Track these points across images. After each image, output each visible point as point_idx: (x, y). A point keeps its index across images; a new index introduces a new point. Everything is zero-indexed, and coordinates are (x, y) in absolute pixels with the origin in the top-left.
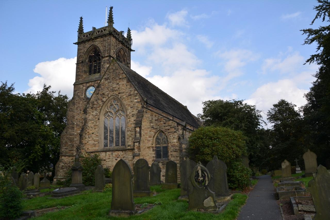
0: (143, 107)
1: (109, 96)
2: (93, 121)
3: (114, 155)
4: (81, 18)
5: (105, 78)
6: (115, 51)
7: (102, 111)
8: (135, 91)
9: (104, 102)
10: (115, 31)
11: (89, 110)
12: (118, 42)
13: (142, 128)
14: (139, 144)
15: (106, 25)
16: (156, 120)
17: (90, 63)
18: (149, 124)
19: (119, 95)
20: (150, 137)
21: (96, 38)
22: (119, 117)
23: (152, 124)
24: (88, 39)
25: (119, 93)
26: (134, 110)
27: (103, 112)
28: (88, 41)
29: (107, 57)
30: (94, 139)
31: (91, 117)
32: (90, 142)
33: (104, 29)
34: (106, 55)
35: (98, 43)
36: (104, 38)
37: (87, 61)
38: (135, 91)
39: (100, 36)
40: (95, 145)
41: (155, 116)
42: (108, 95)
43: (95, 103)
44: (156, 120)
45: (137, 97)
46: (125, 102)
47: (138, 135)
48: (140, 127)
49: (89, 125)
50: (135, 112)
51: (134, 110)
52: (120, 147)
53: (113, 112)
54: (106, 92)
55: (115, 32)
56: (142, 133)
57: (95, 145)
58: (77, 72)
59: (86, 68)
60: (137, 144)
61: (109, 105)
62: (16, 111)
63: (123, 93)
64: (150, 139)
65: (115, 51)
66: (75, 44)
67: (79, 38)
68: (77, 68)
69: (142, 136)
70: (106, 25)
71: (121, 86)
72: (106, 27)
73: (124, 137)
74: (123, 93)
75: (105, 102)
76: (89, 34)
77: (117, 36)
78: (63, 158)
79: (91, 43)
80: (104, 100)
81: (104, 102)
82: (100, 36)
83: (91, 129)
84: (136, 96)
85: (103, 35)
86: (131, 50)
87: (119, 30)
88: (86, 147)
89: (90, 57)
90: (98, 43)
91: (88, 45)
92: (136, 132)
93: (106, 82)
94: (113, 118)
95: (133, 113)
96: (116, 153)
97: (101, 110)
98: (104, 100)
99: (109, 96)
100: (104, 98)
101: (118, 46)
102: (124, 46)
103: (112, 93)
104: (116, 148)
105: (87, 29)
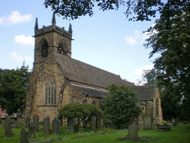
0: (65, 82)
1: (48, 74)
2: (39, 89)
3: (50, 109)
4: (37, 19)
5: (46, 63)
6: (57, 42)
7: (44, 83)
8: (61, 72)
9: (45, 78)
10: (57, 28)
11: (38, 82)
12: (60, 36)
13: (64, 95)
14: (61, 104)
15: (51, 24)
16: (72, 90)
17: (43, 49)
18: (68, 92)
19: (53, 74)
20: (68, 100)
21: (45, 33)
22: (101, 83)
23: (69, 93)
24: (40, 34)
25: (53, 73)
26: (61, 84)
27: (45, 83)
28: (41, 35)
29: (51, 46)
30: (40, 99)
31: (38, 86)
32: (38, 100)
33: (50, 27)
34: (51, 45)
35: (46, 37)
36: (50, 33)
37: (40, 48)
38: (61, 72)
39: (47, 32)
40: (40, 102)
41: (72, 88)
42: (47, 73)
43: (41, 77)
44: (72, 90)
45: (62, 76)
46: (57, 79)
47: (61, 99)
48: (62, 94)
49: (38, 91)
50: (61, 85)
51: (61, 84)
52: (54, 104)
53: (50, 84)
54: (46, 71)
55: (57, 29)
56: (64, 97)
57: (40, 102)
58: (35, 56)
59: (40, 54)
60: (60, 104)
61: (48, 79)
62: (173, 30)
63: (55, 73)
64: (68, 101)
65: (57, 42)
66: (33, 37)
67: (35, 32)
68: (35, 53)
69: (64, 99)
70: (51, 24)
71: (54, 68)
72: (51, 26)
73: (56, 99)
74: (55, 73)
75: (46, 77)
76: (41, 30)
77: (59, 31)
78: (27, 108)
79: (42, 36)
80: (45, 76)
81: (45, 78)
82: (47, 32)
83: (38, 93)
84: (62, 75)
85: (49, 32)
86: (72, 40)
87: (61, 27)
88: (36, 103)
89: (42, 46)
90: (46, 37)
91: (41, 38)
92: (60, 96)
93: (47, 65)
94: (101, 83)
95: (60, 85)
96: (51, 108)
97: (43, 82)
98: (45, 76)
99: (48, 74)
100: (45, 75)
101: (60, 38)
102: (65, 37)
103: (49, 73)
104: (52, 104)
105: (40, 27)
